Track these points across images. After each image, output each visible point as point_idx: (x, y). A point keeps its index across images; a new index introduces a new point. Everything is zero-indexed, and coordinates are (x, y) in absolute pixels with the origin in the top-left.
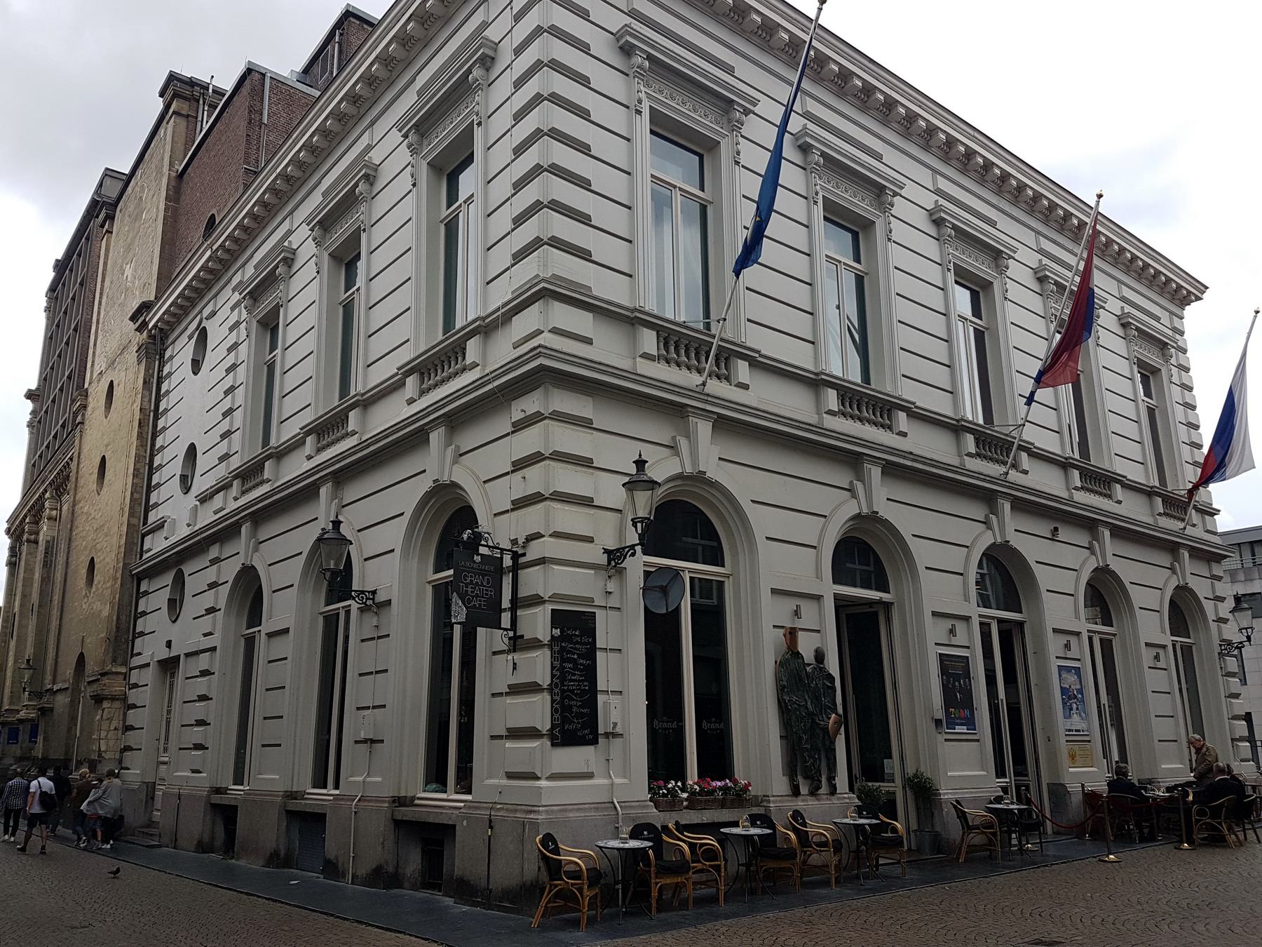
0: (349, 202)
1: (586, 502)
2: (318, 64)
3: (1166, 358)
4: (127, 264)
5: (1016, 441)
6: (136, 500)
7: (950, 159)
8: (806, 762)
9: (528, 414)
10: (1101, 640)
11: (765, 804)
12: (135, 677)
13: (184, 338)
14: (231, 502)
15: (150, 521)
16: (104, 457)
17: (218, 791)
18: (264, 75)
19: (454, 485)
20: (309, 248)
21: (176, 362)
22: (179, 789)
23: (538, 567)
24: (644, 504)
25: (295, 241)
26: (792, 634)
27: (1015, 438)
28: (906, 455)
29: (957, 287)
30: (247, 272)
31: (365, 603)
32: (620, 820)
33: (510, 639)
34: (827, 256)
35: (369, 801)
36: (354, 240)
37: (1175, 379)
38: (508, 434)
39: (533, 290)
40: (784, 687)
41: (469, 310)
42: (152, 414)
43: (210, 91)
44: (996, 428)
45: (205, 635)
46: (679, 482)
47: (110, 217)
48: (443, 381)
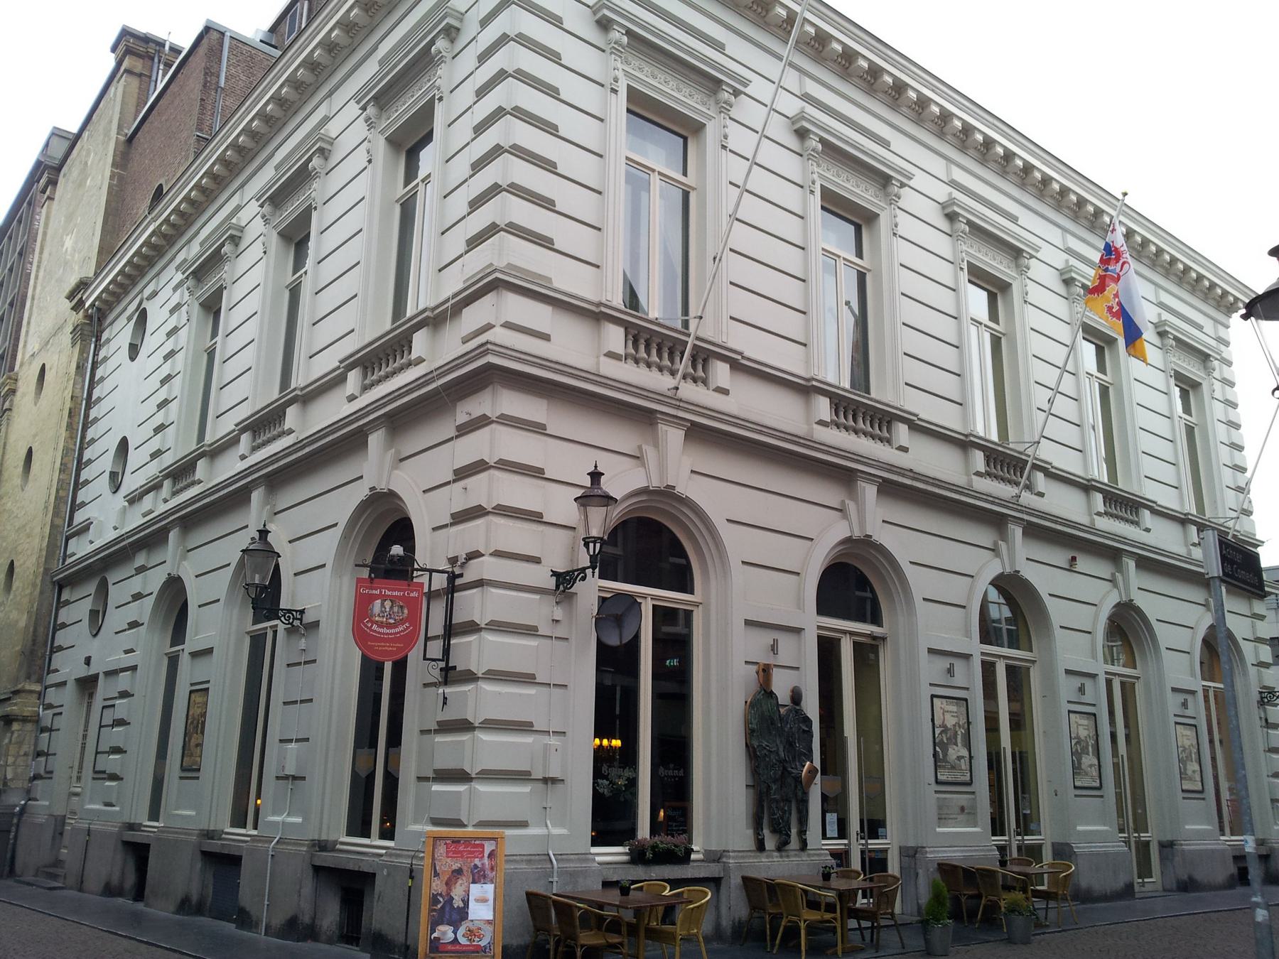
0: (301, 177)
1: (534, 517)
2: (286, 22)
3: (1209, 370)
4: (67, 235)
5: (1030, 460)
6: (61, 498)
7: (966, 148)
8: (774, 814)
9: (473, 417)
10: (1123, 684)
11: (724, 860)
12: (52, 696)
13: (123, 320)
14: (159, 505)
15: (75, 523)
16: (31, 448)
17: (132, 827)
18: (223, 34)
19: (392, 495)
20: (258, 226)
21: (113, 346)
22: (90, 824)
23: (474, 591)
24: (599, 522)
25: (243, 217)
26: (766, 671)
27: (1029, 456)
28: (906, 473)
29: (970, 286)
30: (192, 250)
31: (291, 624)
32: (555, 874)
33: (441, 669)
34: (823, 249)
35: (288, 844)
36: (304, 218)
37: (1218, 395)
38: (451, 439)
39: (485, 281)
40: (753, 731)
41: (422, 298)
42: (84, 402)
43: (167, 48)
44: (1011, 446)
45: (127, 652)
46: (644, 498)
47: (53, 182)
48: (387, 377)
